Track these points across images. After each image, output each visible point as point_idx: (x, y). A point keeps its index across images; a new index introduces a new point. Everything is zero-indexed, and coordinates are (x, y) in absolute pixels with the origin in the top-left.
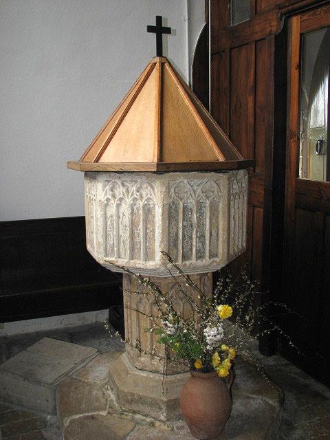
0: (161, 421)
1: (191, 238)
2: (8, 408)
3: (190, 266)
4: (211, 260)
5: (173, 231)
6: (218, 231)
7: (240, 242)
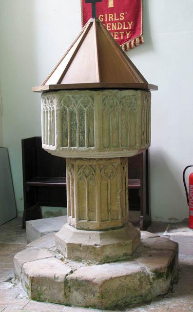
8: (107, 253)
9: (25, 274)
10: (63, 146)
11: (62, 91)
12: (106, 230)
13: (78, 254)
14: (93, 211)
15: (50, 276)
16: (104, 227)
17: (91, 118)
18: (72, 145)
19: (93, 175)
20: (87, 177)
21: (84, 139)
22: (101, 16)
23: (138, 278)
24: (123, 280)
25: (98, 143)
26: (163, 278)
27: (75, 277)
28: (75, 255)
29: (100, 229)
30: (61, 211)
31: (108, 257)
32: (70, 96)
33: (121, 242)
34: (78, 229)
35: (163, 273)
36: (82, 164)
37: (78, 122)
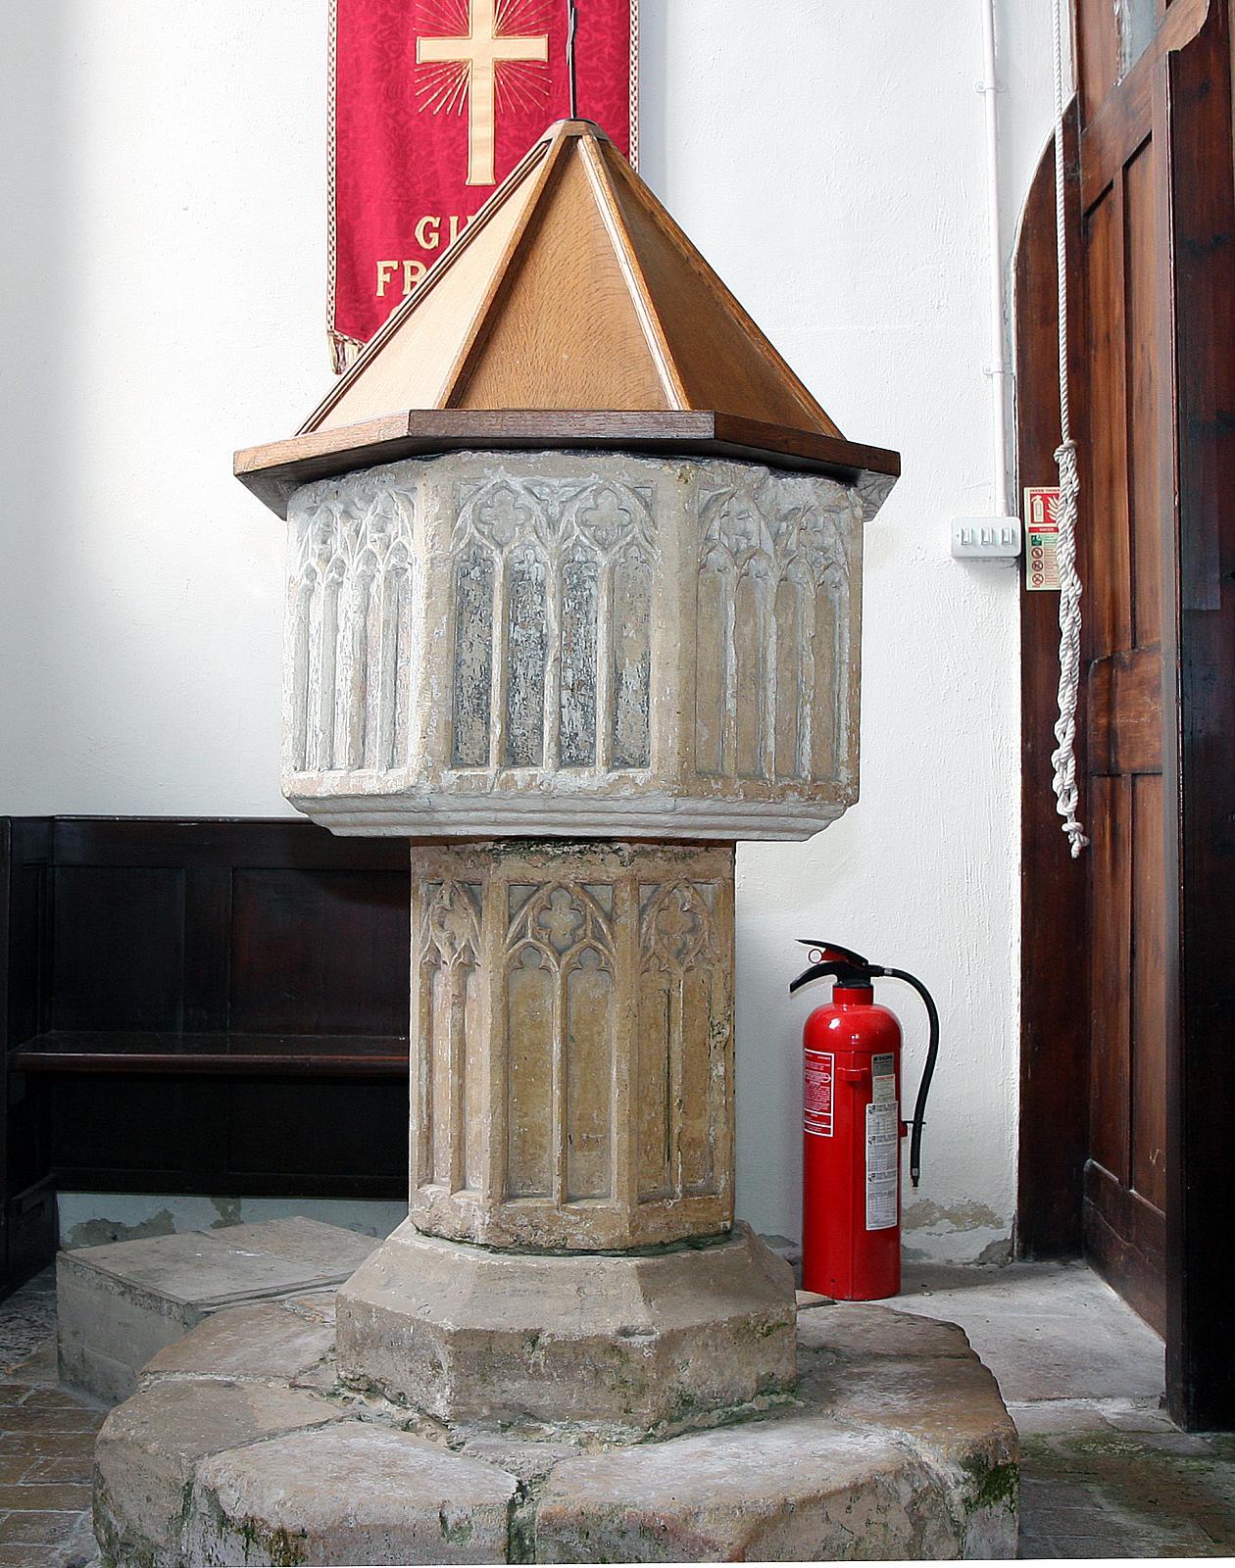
0: (435, 1418)
1: (538, 686)
2: (70, 1401)
3: (529, 786)
4: (615, 775)
5: (472, 657)
6: (647, 670)
7: (1079, 1262)
8: (686, 1375)
9: (224, 1521)
10: (456, 761)
11: (466, 456)
12: (661, 1248)
13: (517, 1389)
14: (588, 1144)
15: (413, 1515)
16: (655, 1229)
17: (632, 608)
18: (512, 756)
19: (601, 938)
20: (559, 953)
21: (589, 725)
22: (429, 224)
23: (905, 1502)
24: (836, 1512)
25: (673, 743)
26: (1006, 1498)
27: (574, 1509)
28: (497, 1400)
29: (630, 1241)
30: (167, 1216)
31: (687, 1402)
32: (516, 483)
33: (749, 1310)
34: (495, 1250)
35: (1006, 1466)
36: (537, 876)
37: (553, 625)
